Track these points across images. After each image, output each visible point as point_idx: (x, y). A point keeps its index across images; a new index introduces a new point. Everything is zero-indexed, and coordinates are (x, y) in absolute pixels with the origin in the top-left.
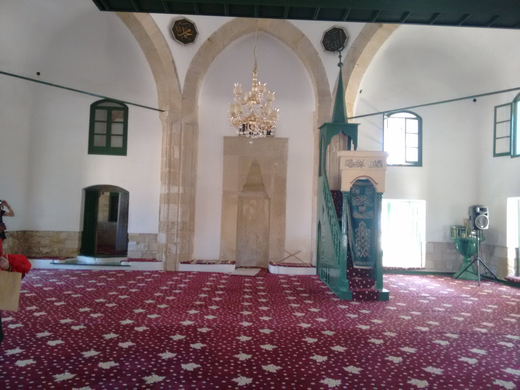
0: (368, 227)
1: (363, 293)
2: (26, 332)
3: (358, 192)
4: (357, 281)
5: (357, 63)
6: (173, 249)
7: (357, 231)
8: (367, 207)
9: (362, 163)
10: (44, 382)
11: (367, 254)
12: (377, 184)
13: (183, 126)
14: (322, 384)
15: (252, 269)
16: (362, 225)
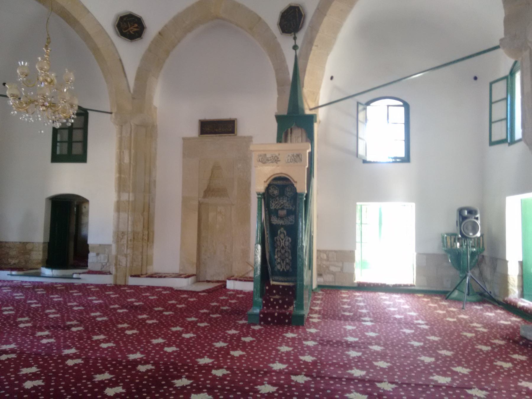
1: (272, 315)
3: (276, 192)
5: (315, 43)
6: (123, 261)
7: (277, 240)
8: (287, 210)
9: (278, 158)
10: (165, 387)
11: (288, 267)
12: (296, 182)
13: (133, 128)
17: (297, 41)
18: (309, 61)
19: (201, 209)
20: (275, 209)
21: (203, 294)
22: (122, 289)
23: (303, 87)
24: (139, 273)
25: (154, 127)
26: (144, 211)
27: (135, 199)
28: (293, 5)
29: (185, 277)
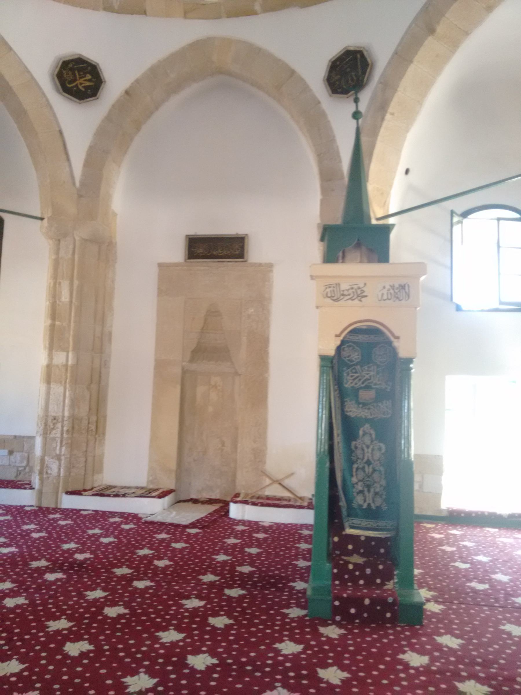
0: (380, 438)
1: (357, 602)
2: (51, 542)
3: (356, 356)
4: (351, 567)
5: (390, 110)
6: (54, 467)
7: (356, 447)
9: (363, 291)
11: (379, 501)
12: (398, 338)
13: (78, 243)
14: (401, 659)
15: (199, 506)
16: (366, 435)
17: (360, 104)
18: (379, 138)
19: (187, 381)
20: (353, 387)
21: (194, 531)
22: (51, 516)
23: (367, 181)
24: (79, 487)
25: (111, 245)
26: (91, 382)
27: (77, 364)
28: (352, 49)
29: (160, 497)
